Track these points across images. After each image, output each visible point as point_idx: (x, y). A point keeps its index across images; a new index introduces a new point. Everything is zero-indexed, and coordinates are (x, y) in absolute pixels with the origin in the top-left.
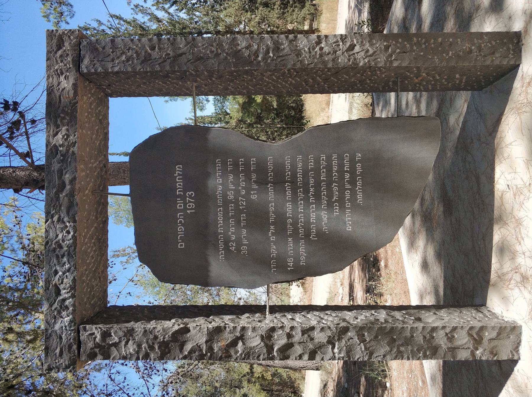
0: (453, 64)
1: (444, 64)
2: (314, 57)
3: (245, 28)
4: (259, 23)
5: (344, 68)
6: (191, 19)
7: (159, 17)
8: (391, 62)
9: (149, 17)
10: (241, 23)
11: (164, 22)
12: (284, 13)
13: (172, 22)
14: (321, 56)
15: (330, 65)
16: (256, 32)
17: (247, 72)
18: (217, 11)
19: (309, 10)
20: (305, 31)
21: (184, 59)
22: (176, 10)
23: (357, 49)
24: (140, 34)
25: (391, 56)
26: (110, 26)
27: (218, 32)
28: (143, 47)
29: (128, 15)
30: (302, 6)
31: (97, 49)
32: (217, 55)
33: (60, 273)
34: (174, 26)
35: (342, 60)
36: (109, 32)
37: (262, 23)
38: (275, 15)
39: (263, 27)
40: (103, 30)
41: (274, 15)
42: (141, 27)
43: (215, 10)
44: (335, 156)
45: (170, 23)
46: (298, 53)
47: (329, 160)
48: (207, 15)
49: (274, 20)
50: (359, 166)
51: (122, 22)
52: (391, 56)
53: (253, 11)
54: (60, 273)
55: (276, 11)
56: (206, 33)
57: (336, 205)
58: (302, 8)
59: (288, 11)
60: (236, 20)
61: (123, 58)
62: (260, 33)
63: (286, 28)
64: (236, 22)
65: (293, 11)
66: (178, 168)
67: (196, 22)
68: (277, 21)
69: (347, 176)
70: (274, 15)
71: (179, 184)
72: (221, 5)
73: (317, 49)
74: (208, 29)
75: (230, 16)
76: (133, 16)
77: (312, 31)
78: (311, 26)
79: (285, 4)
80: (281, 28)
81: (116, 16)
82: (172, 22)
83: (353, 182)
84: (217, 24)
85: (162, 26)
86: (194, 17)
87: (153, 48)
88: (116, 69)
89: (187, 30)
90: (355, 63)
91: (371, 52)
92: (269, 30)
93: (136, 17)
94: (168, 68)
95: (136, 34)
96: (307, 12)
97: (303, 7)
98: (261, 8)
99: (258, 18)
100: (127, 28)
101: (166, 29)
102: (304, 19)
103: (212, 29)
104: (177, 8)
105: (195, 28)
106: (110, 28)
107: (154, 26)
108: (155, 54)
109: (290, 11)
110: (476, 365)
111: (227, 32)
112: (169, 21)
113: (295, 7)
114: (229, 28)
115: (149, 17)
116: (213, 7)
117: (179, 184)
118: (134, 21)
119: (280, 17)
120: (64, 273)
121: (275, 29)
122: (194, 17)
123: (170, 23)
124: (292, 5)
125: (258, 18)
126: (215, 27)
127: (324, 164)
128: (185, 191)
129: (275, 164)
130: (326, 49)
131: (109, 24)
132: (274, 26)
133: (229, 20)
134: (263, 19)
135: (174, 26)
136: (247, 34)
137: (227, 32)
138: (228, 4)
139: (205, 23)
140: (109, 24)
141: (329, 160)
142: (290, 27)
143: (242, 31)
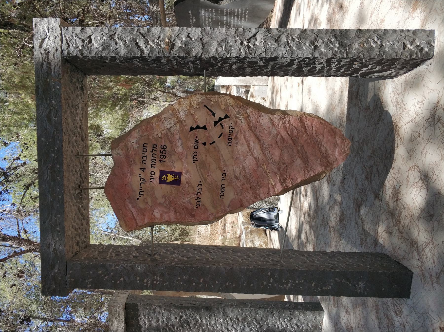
44: (240, 9)
47: (238, 10)
50: (247, 12)
57: (236, 17)
66: (190, 12)
69: (243, 14)
71: (191, 15)
83: (245, 16)
110: (431, 276)
117: (191, 15)
127: (236, 11)
128: (192, 17)
129: (347, 326)
141: (238, 10)
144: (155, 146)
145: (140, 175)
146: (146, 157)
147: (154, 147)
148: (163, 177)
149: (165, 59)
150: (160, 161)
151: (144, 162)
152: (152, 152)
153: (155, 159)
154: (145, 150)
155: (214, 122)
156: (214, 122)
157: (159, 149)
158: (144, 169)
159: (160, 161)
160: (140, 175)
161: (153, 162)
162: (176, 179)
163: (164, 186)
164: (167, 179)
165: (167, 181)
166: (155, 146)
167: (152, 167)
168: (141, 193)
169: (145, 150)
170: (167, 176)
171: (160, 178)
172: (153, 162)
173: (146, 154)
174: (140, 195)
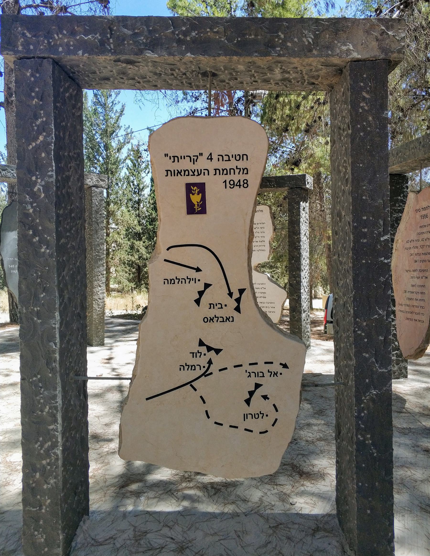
0: (94, 322)
1: (94, 320)
2: (97, 273)
3: (112, 228)
4: (116, 241)
5: (93, 284)
6: (120, 180)
7: (122, 150)
8: (95, 301)
9: (122, 141)
10: (117, 225)
11: (118, 154)
12: (124, 263)
13: (117, 162)
14: (97, 275)
15: (94, 279)
16: (108, 239)
17: (92, 248)
18: (127, 204)
19: (126, 286)
20: (109, 283)
21: (97, 226)
22: (128, 165)
23: (100, 288)
24: (107, 130)
25: (97, 300)
26: (114, 103)
27: (108, 204)
28: (101, 211)
29: (123, 122)
30: (130, 280)
31: (100, 194)
32: (98, 238)
33: (12, 172)
34: (114, 164)
35: (95, 283)
36: (110, 100)
37: (117, 244)
38: (123, 256)
39: (113, 245)
40: (111, 96)
41: (123, 255)
42: (114, 132)
43: (128, 201)
45: (117, 161)
46: (98, 267)
48: (124, 194)
49: (119, 255)
51: (118, 115)
52: (97, 300)
53: (127, 235)
54: (12, 172)
55: (126, 257)
56: (108, 193)
58: (128, 280)
59: (126, 267)
60: (119, 221)
61: (97, 204)
62: (107, 242)
63: (111, 266)
64: (117, 220)
65: (126, 272)
67: (117, 184)
68: (118, 258)
70: (123, 255)
72: (132, 207)
73: (100, 274)
74: (111, 195)
75: (122, 215)
76: (123, 127)
77: (109, 290)
78: (114, 290)
79: (132, 265)
80: (112, 261)
81: (123, 111)
82: (117, 162)
84: (116, 203)
85: (114, 151)
86: (122, 183)
87: (100, 215)
88: (93, 201)
89: (111, 176)
90: (94, 288)
91: (98, 293)
92: (110, 250)
93: (123, 129)
94: (93, 220)
95: (107, 126)
96: (125, 285)
97: (130, 281)
98: (129, 243)
99: (121, 241)
100: (112, 118)
101: (111, 155)
102: (119, 283)
103: (112, 197)
104: (130, 166)
105: (112, 182)
106: (113, 102)
107: (114, 144)
108: (98, 216)
109: (126, 269)
111: (108, 212)
112: (119, 159)
113: (129, 274)
114: (112, 214)
115: (122, 141)
116: (131, 200)
118: (118, 126)
119: (121, 260)
120: (12, 173)
121: (111, 256)
122: (122, 183)
123: (117, 161)
124: (131, 271)
125: (121, 241)
126: (112, 202)
130: (99, 277)
131: (117, 102)
132: (113, 255)
133: (119, 213)
134: (119, 245)
135: (114, 164)
136: (107, 231)
137: (108, 212)
138: (133, 214)
139: (117, 193)
140: (117, 102)
142: (112, 269)
143: (109, 226)
144: (245, 171)
145: (201, 154)
146: (229, 160)
147: (244, 170)
148: (195, 188)
149: (338, 51)
150: (225, 181)
151: (221, 158)
152: (186, 365)
153: (227, 174)
154: (238, 158)
155: (235, 309)
156: (235, 309)
157: (242, 177)
158: (211, 159)
159: (225, 181)
160: (201, 154)
161: (223, 170)
162: (196, 207)
163: (184, 190)
164: (193, 194)
165: (191, 195)
166: (245, 171)
167: (215, 170)
168: (176, 158)
169: (238, 158)
170: (198, 194)
171: (194, 185)
172: (223, 170)
173: (233, 159)
174: (172, 158)
